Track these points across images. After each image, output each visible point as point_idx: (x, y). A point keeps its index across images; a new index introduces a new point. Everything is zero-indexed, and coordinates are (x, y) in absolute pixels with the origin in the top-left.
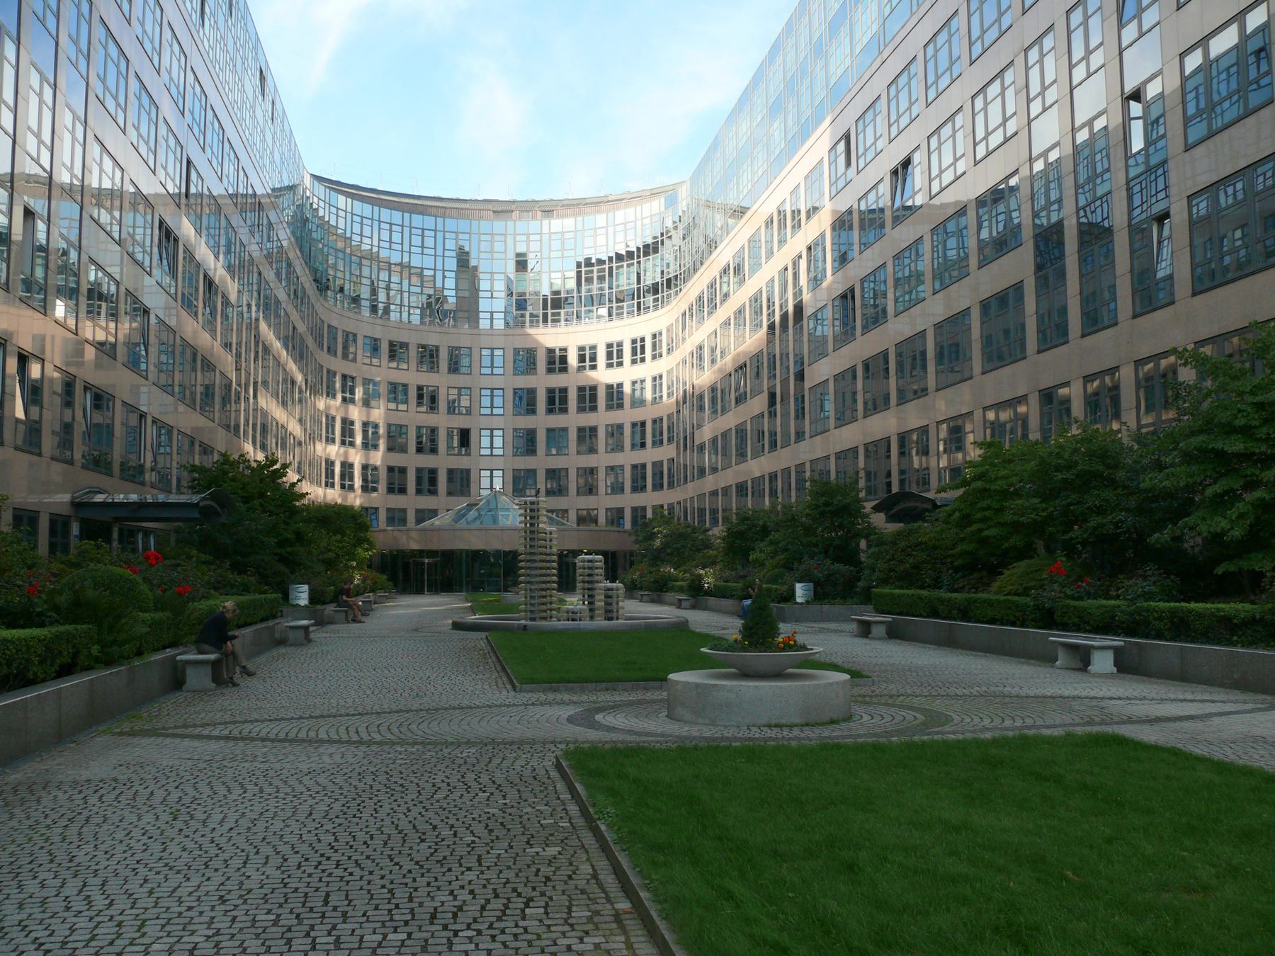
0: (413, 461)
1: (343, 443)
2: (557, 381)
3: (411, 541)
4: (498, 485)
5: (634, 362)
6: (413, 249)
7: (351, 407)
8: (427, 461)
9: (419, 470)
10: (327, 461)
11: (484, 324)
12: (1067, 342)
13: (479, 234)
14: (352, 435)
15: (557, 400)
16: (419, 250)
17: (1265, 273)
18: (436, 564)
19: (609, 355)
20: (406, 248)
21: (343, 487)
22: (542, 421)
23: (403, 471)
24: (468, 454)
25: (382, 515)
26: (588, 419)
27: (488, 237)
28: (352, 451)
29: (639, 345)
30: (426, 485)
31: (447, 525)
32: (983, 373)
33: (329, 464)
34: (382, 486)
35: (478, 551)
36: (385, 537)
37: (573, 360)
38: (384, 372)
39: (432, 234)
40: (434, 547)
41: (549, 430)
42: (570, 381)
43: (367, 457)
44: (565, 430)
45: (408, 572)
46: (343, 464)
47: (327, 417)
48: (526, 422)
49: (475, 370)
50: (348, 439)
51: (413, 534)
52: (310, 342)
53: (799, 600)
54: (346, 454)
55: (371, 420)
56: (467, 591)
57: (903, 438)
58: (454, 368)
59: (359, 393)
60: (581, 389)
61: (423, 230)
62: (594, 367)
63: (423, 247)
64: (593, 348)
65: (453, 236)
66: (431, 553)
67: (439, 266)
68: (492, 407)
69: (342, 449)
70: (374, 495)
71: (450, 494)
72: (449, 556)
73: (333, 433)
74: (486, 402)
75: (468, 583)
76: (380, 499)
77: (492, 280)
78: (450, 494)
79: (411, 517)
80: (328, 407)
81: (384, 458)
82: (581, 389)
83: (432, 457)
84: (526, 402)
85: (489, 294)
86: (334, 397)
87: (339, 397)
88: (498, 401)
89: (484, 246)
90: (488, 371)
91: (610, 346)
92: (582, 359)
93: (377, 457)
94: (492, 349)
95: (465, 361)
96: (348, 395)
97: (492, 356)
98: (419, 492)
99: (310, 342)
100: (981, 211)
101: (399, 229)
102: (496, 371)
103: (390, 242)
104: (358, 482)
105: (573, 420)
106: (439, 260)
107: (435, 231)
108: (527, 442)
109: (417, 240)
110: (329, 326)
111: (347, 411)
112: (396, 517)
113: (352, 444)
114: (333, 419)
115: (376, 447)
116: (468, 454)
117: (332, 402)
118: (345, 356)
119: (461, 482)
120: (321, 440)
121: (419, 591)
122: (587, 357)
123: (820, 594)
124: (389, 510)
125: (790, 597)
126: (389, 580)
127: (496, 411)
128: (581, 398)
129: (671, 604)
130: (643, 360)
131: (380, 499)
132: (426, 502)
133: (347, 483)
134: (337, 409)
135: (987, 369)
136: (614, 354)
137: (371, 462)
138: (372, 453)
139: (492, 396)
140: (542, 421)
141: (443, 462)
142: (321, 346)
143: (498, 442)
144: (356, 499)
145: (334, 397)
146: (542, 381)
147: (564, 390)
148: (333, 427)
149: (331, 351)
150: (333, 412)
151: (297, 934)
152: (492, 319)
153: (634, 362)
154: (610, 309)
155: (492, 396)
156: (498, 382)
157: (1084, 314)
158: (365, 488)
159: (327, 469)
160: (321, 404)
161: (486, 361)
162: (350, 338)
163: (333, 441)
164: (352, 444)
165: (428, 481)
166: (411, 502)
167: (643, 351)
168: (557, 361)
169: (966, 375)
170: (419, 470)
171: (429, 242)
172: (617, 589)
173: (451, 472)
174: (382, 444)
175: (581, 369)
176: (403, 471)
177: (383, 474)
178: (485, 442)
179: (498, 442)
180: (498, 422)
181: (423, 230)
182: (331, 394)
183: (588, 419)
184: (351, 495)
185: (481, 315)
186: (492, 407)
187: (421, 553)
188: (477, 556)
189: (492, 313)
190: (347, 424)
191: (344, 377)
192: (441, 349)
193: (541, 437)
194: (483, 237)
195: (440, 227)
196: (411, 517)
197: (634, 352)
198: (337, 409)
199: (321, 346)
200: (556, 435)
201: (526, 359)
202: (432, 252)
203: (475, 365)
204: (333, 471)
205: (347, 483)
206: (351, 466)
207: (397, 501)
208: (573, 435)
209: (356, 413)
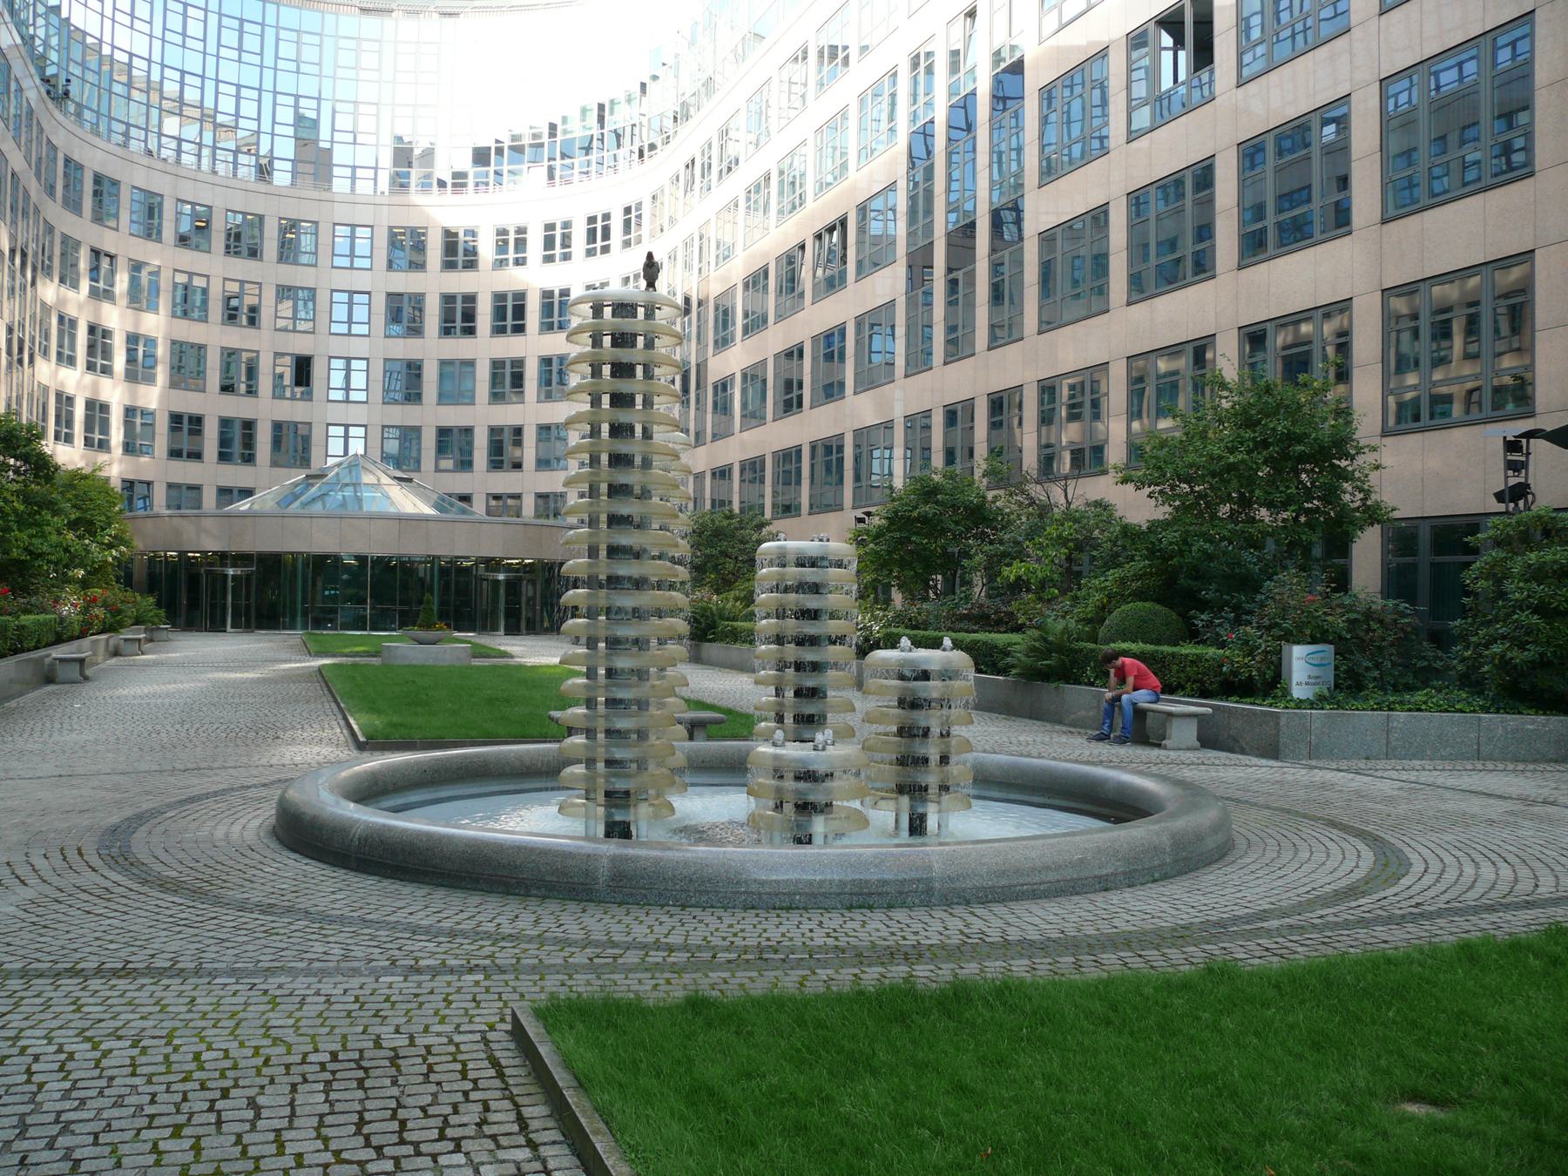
0: (212, 405)
1: (91, 367)
2: (460, 282)
3: (205, 537)
4: (357, 447)
5: (590, 253)
6: (223, 52)
7: (106, 307)
8: (236, 407)
9: (225, 423)
10: (59, 395)
11: (340, 185)
12: (1350, 233)
13: (337, 37)
14: (107, 353)
15: (459, 316)
16: (234, 55)
17: (1401, 222)
18: (248, 577)
19: (549, 243)
20: (212, 48)
21: (88, 442)
22: (432, 348)
23: (197, 421)
24: (307, 396)
25: (160, 495)
26: (509, 347)
27: (352, 44)
28: (105, 382)
29: (599, 225)
30: (237, 448)
31: (268, 512)
32: (906, 376)
33: (65, 401)
34: (161, 443)
35: (325, 557)
36: (162, 533)
37: (486, 250)
38: (163, 257)
39: (258, 29)
40: (247, 547)
41: (443, 363)
42: (484, 283)
43: (133, 395)
44: (471, 363)
45: (195, 594)
46: (90, 404)
47: (61, 319)
48: (406, 348)
49: (324, 260)
50: (100, 362)
51: (208, 523)
52: (34, 188)
53: (1298, 692)
54: (95, 387)
55: (142, 331)
56: (305, 627)
57: (1047, 389)
58: (288, 252)
59: (122, 283)
60: (500, 297)
61: (242, 21)
62: (520, 262)
63: (240, 49)
64: (521, 231)
65: (293, 36)
66: (241, 559)
67: (268, 85)
68: (350, 322)
69: (89, 378)
70: (144, 459)
71: (274, 464)
72: (271, 566)
73: (73, 347)
74: (340, 312)
75: (305, 614)
76: (156, 467)
77: (355, 114)
78: (274, 464)
79: (209, 499)
80: (62, 301)
81: (162, 397)
82: (500, 297)
83: (252, 264)
84: (403, 313)
85: (350, 138)
86: (75, 285)
87: (85, 285)
88: (360, 313)
89: (346, 58)
90: (345, 262)
91: (550, 227)
92: (502, 247)
93: (152, 396)
94: (353, 226)
95: (306, 242)
96: (101, 285)
97: (353, 237)
98: (224, 457)
99: (34, 188)
100: (1135, 55)
101: (198, 82)
102: (358, 263)
103: (240, 49)
104: (117, 436)
105: (485, 347)
106: (268, 74)
107: (263, 25)
108: (407, 381)
109: (230, 38)
110: (68, 161)
111: (97, 312)
112: (185, 495)
113: (107, 371)
114: (73, 323)
115: (150, 380)
116: (307, 396)
117: (71, 294)
118: (98, 219)
119: (294, 444)
120: (45, 353)
121: (216, 625)
122: (512, 244)
123: (1348, 686)
124: (170, 486)
125: (1271, 684)
126: (159, 605)
127: (356, 329)
128: (499, 313)
129: (1077, 725)
130: (605, 249)
131: (156, 467)
132: (236, 475)
133: (97, 436)
134: (80, 307)
135: (1134, 299)
136: (556, 242)
137: (141, 403)
138: (143, 389)
139: (351, 304)
140: (432, 348)
141: (266, 409)
142: (51, 191)
143: (358, 380)
144: (115, 467)
145: (75, 285)
146: (434, 283)
147: (470, 299)
148: (73, 337)
149: (73, 205)
150: (72, 311)
151: (51, 1058)
152: (353, 178)
153: (590, 253)
154: (551, 170)
155: (351, 304)
156: (361, 281)
157: (948, 342)
158: (129, 448)
159: (58, 411)
160: (49, 291)
161: (342, 245)
162: (104, 187)
163: (71, 361)
164: (107, 371)
165: (238, 441)
166: (209, 473)
167: (606, 236)
168: (458, 254)
169: (1015, 336)
170: (225, 423)
171: (251, 43)
172: (947, 675)
173: (278, 426)
174: (162, 374)
175: (501, 264)
176: (197, 421)
177: (162, 425)
178: (337, 379)
179: (358, 380)
180: (358, 347)
181: (242, 21)
182: (68, 278)
183: (509, 347)
184: (102, 458)
185: (336, 171)
186: (350, 322)
187: (223, 557)
188: (323, 565)
189: (354, 168)
190: (99, 336)
191: (96, 253)
192: (267, 220)
193: (430, 374)
194: (342, 43)
195: (270, 20)
196: (209, 499)
197: (591, 236)
198: (80, 307)
199: (51, 191)
200: (456, 373)
201: (407, 247)
202: (257, 60)
203: (324, 251)
204: (70, 414)
205: (97, 436)
206: (105, 408)
207: (186, 472)
208: (483, 373)
209: (115, 318)
